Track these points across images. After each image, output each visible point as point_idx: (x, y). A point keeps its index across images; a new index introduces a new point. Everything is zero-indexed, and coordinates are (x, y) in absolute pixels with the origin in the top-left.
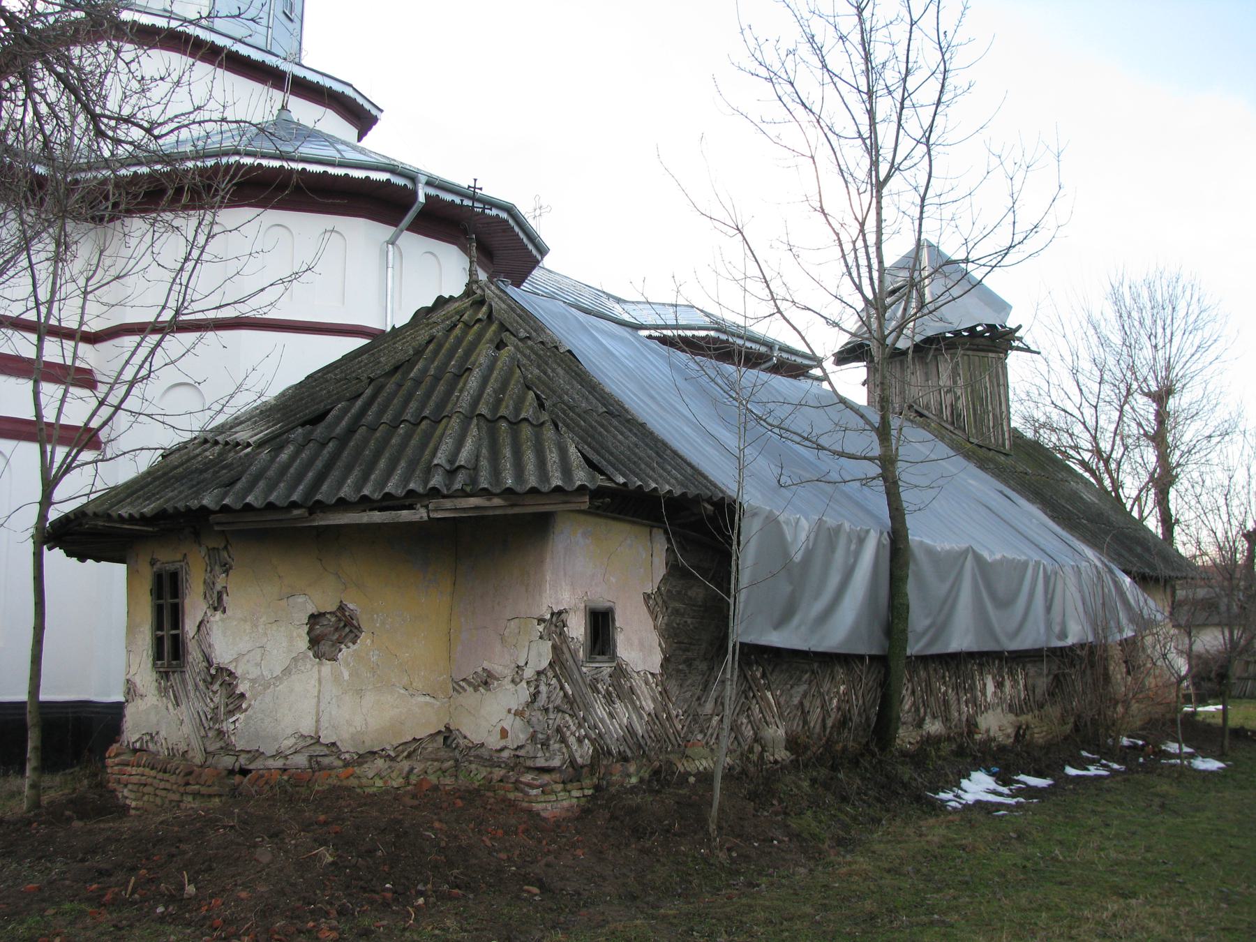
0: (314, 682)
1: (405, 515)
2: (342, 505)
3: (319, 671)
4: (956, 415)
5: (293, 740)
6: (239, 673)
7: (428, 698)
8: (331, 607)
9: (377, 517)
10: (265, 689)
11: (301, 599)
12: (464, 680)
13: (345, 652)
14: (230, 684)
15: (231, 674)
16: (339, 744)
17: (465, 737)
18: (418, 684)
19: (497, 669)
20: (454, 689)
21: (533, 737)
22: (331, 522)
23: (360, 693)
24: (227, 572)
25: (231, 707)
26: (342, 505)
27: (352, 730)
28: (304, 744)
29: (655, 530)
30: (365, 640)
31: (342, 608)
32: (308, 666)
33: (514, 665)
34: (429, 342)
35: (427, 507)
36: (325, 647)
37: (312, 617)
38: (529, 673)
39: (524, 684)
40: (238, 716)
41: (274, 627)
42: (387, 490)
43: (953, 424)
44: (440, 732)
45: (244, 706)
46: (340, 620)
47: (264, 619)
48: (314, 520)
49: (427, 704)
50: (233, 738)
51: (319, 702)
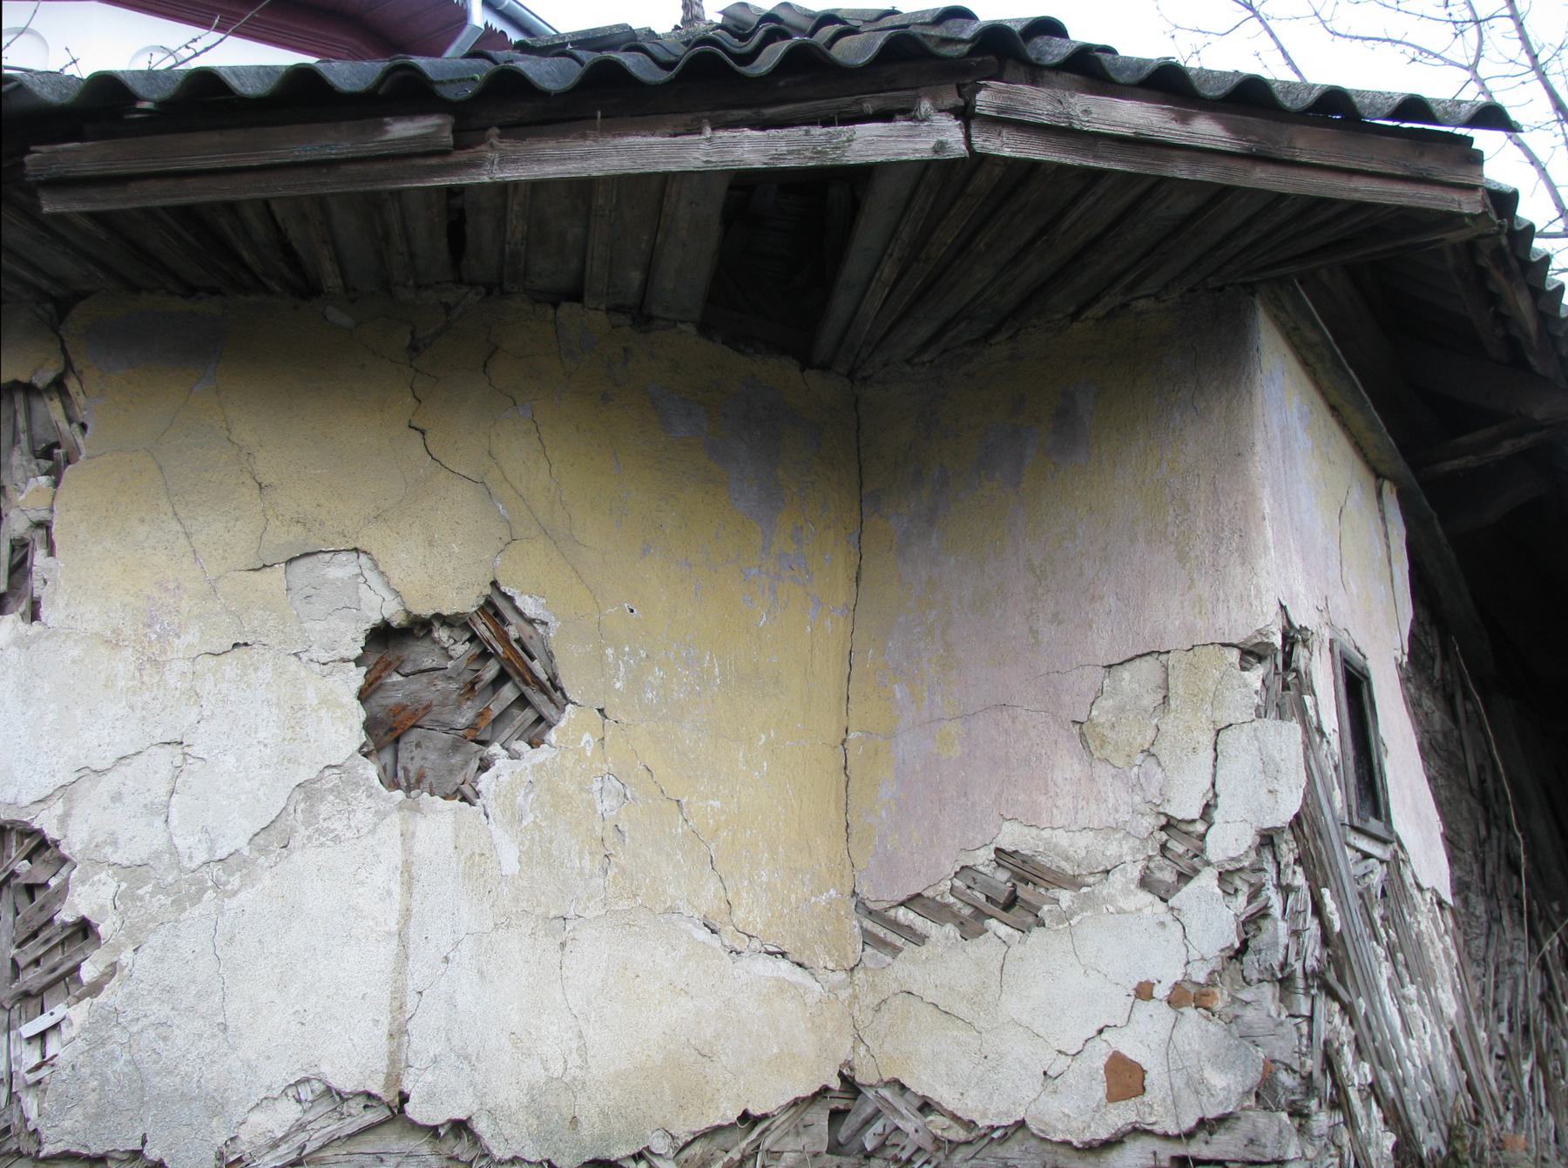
0: (385, 875)
1: (870, 143)
3: (406, 837)
5: (289, 1112)
6: (73, 843)
7: (784, 965)
8: (462, 600)
10: (179, 905)
11: (341, 570)
12: (912, 901)
13: (509, 771)
14: (31, 890)
15: (41, 846)
16: (481, 1126)
17: (926, 1106)
18: (752, 913)
19: (1057, 837)
20: (870, 939)
21: (1264, 1093)
22: (551, 171)
23: (559, 926)
24: (56, 474)
25: (32, 978)
27: (533, 1072)
28: (333, 1127)
30: (572, 728)
31: (491, 610)
32: (362, 817)
33: (1149, 822)
35: (965, 114)
36: (421, 753)
37: (383, 637)
38: (1229, 840)
39: (1207, 880)
40: (60, 1010)
41: (230, 666)
44: (824, 1091)
45: (88, 973)
46: (485, 655)
47: (191, 636)
48: (475, 164)
49: (782, 987)
50: (30, 1104)
51: (403, 956)
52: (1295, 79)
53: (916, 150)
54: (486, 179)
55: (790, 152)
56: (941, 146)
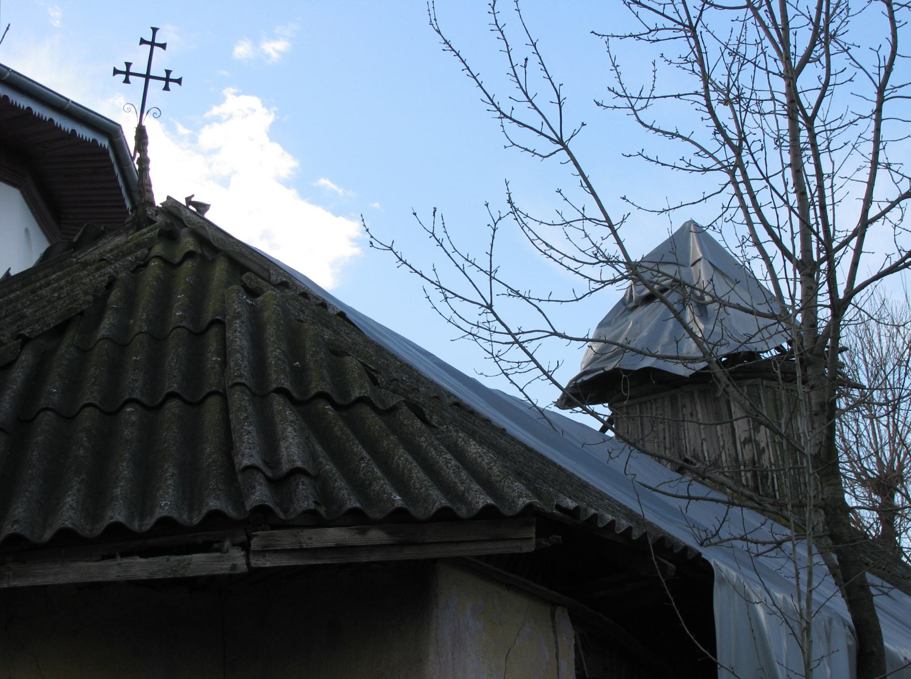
1: (199, 564)
2: (68, 543)
4: (760, 476)
9: (140, 568)
22: (40, 581)
26: (68, 543)
29: (559, 611)
34: (110, 286)
35: (245, 546)
42: (159, 513)
43: (756, 489)
52: (791, 252)
53: (222, 569)
54: (6, 586)
55: (160, 571)
56: (234, 567)
